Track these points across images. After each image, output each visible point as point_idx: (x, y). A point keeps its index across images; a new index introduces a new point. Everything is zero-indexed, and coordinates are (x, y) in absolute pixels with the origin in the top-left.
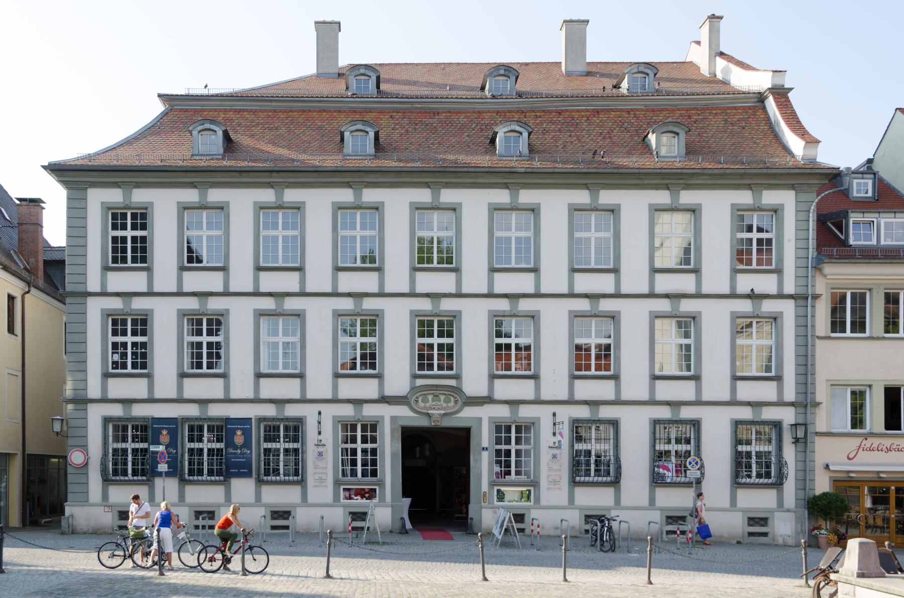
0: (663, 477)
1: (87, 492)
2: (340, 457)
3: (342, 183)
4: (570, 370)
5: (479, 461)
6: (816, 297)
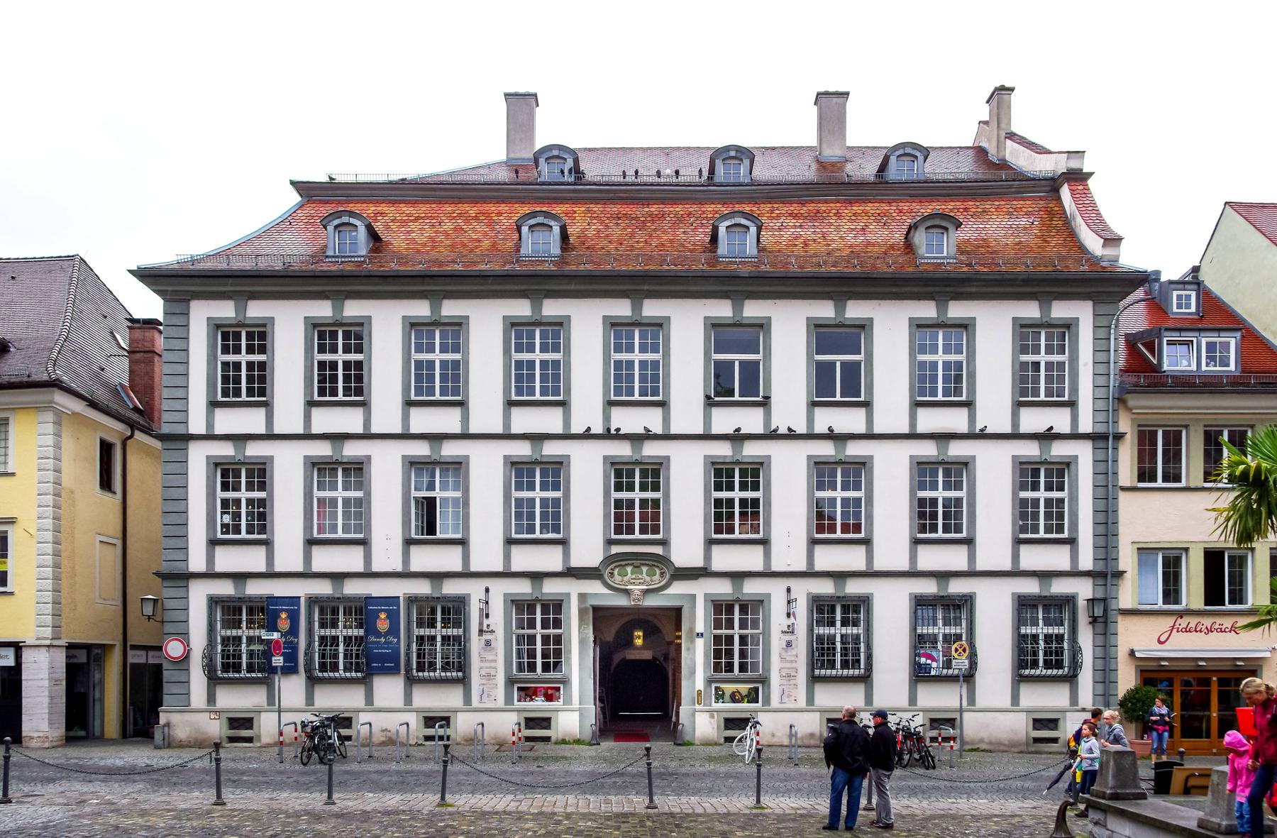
0: (927, 668)
1: (188, 694)
2: (514, 647)
3: (511, 291)
4: (706, 531)
5: (692, 650)
6: (1119, 437)
